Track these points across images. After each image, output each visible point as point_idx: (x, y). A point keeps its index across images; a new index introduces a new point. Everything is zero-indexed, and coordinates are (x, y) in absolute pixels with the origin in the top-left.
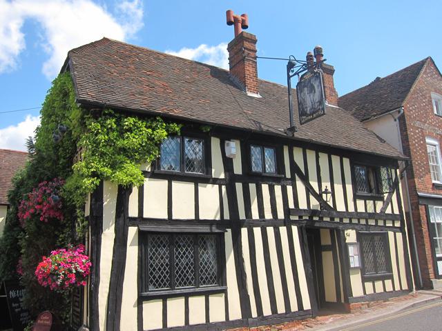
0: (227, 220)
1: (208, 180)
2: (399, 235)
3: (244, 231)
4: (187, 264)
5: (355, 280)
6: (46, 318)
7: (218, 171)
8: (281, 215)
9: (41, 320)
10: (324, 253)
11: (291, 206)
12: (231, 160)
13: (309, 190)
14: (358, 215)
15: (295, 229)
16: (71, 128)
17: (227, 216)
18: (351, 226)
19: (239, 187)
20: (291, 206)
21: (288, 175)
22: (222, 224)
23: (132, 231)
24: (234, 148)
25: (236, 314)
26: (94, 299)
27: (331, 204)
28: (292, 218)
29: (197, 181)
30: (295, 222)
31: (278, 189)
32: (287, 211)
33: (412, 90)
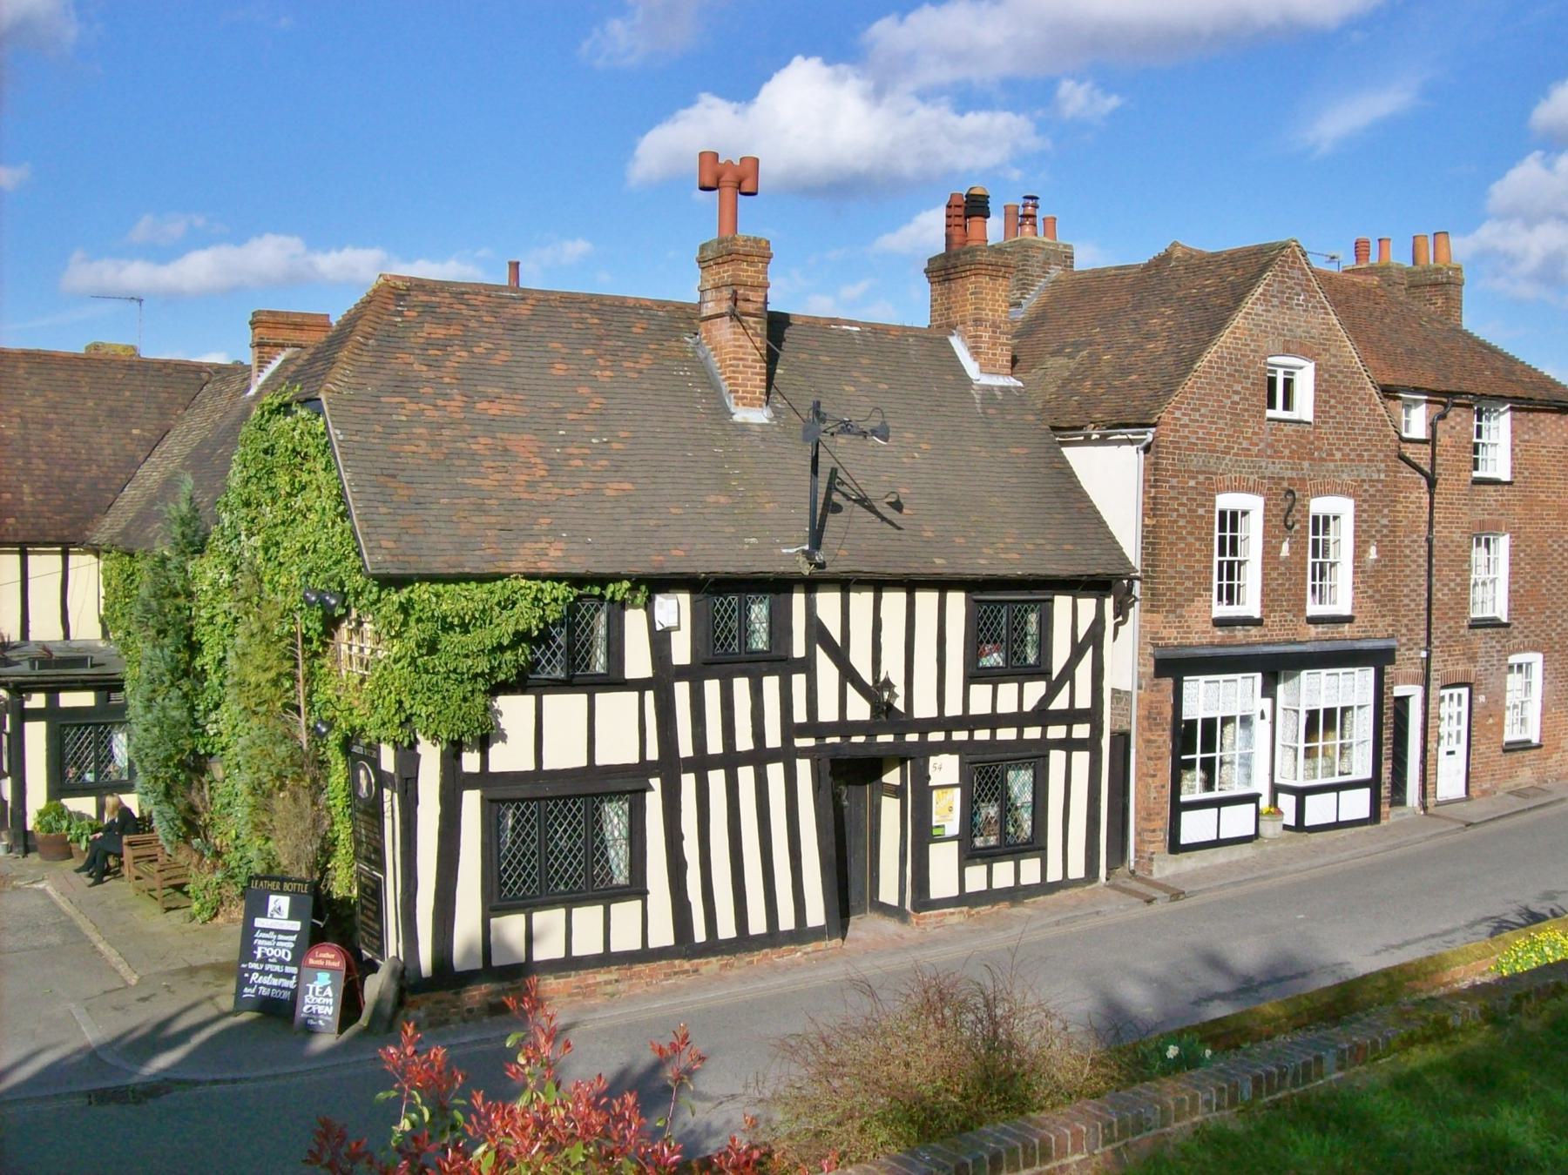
0: (652, 762)
1: (615, 683)
2: (1081, 759)
3: (688, 781)
4: (570, 850)
5: (943, 860)
6: (327, 955)
7: (638, 664)
8: (773, 739)
9: (316, 959)
10: (998, 738)
11: (800, 716)
12: (667, 632)
13: (848, 674)
14: (968, 721)
15: (804, 767)
16: (1366, 1020)
17: (653, 754)
18: (947, 747)
19: (682, 690)
20: (800, 716)
21: (799, 651)
22: (643, 769)
23: (471, 801)
24: (674, 609)
25: (662, 934)
26: (831, 825)
27: (899, 704)
28: (800, 743)
29: (593, 685)
30: (804, 753)
31: (771, 684)
32: (790, 729)
33: (1201, 365)
